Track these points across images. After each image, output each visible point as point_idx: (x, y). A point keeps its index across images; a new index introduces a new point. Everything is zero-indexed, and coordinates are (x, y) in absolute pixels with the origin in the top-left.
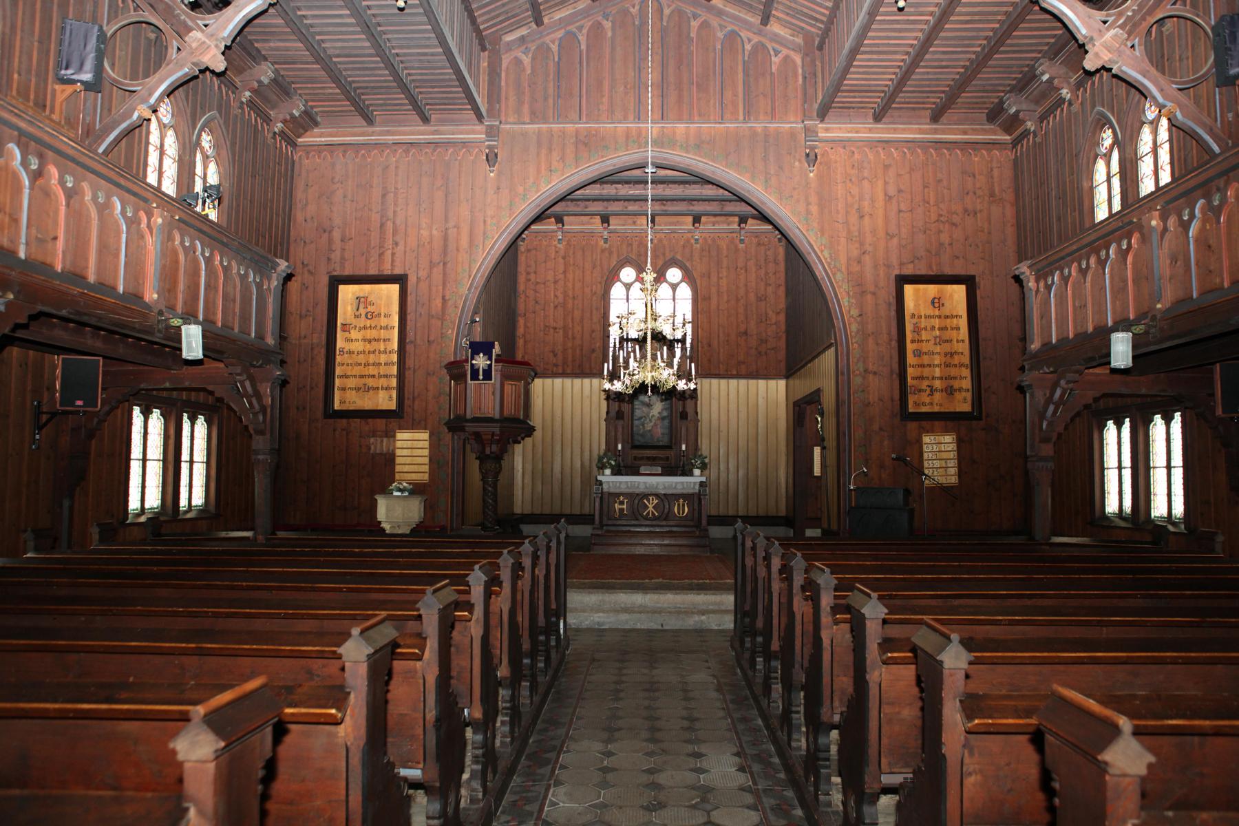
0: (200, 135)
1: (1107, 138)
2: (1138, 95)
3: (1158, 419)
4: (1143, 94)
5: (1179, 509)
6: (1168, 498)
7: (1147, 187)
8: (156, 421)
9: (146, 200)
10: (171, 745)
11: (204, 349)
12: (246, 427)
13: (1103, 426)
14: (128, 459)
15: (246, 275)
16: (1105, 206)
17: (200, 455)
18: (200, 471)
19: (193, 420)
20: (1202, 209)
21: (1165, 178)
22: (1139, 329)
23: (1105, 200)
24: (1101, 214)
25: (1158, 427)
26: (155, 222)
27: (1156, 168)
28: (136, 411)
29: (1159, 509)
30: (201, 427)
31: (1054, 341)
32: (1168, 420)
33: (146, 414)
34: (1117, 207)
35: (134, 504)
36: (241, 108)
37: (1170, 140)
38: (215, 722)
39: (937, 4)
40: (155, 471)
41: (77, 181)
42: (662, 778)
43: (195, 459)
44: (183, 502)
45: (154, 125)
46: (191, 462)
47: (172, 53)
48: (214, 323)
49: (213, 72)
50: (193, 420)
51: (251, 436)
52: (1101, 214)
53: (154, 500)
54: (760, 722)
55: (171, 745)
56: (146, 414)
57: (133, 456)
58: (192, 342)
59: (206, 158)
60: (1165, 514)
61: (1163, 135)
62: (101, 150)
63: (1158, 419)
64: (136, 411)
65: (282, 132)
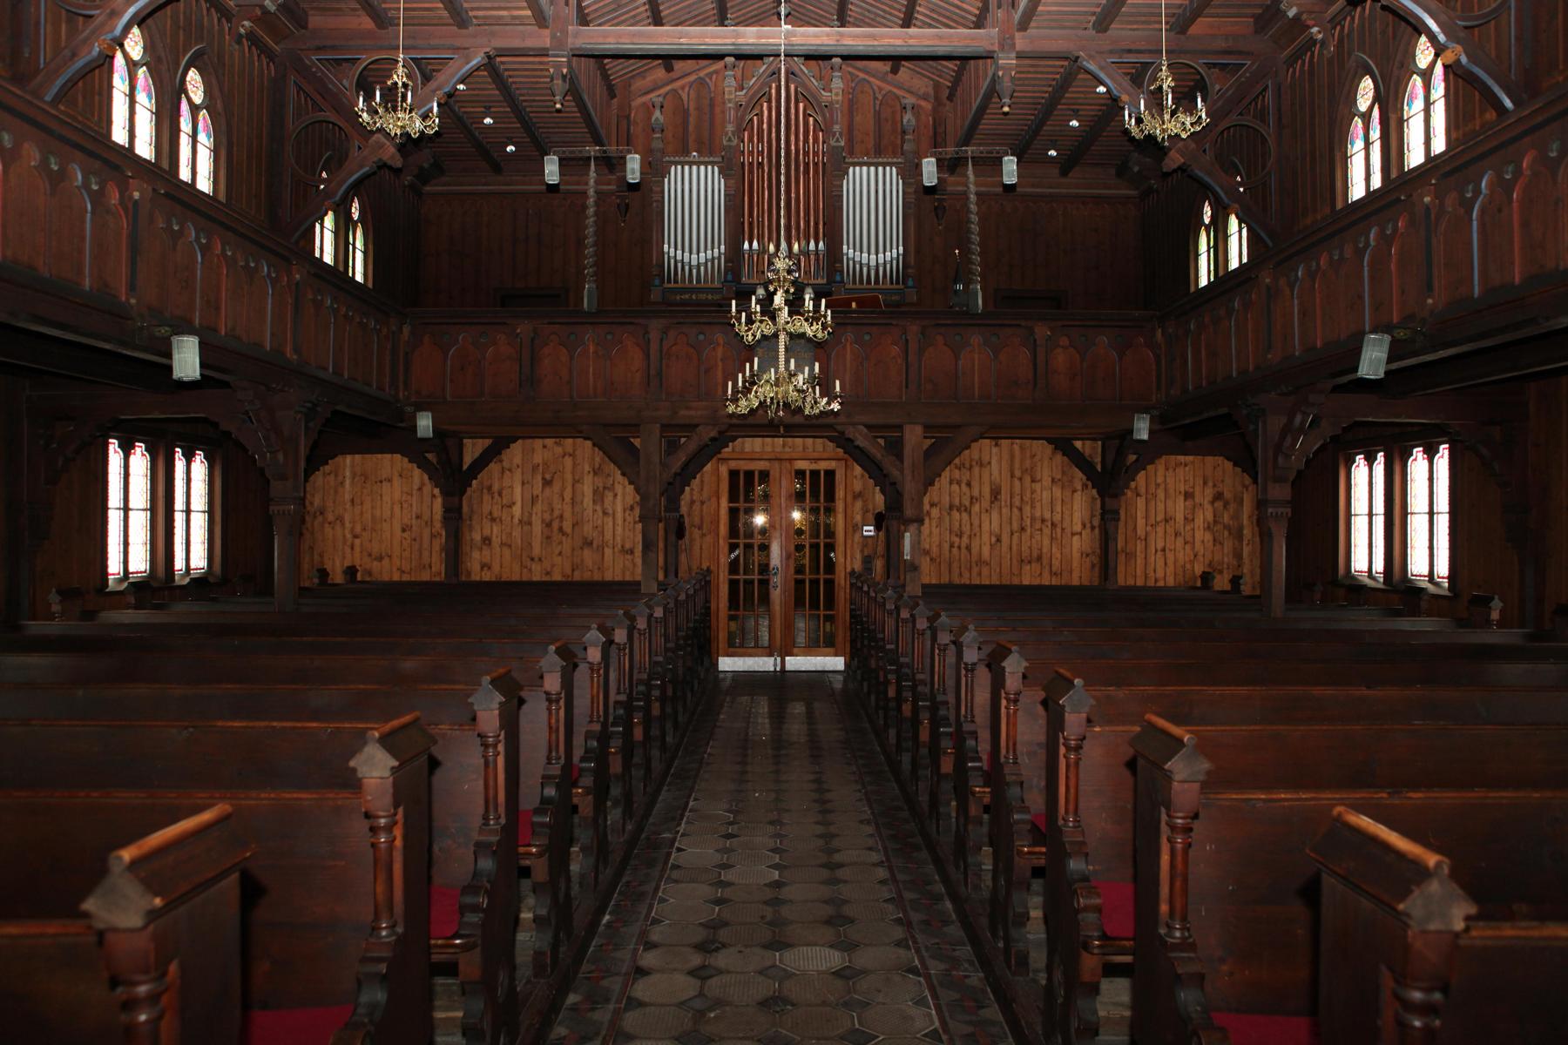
0: (127, 30)
1: (1366, 87)
2: (1410, 29)
3: (1418, 453)
4: (1419, 29)
5: (1442, 568)
6: (1429, 555)
7: (1415, 157)
8: (140, 461)
9: (116, 168)
10: (352, 764)
11: (202, 365)
12: (262, 470)
13: (1350, 462)
14: (105, 509)
15: (102, 192)
16: (1363, 184)
17: (199, 501)
18: (199, 522)
19: (189, 458)
20: (1490, 185)
21: (1439, 146)
22: (1155, 413)
23: (1362, 175)
24: (1357, 192)
25: (1418, 465)
26: (131, 197)
27: (1426, 131)
28: (114, 448)
29: (1418, 565)
30: (199, 468)
31: (1517, 280)
32: (1431, 453)
33: (127, 450)
34: (1376, 182)
35: (114, 566)
36: (239, 42)
37: (1446, 96)
38: (386, 741)
39: (1098, 5)
40: (140, 523)
41: (209, 238)
42: (786, 893)
43: (193, 507)
44: (179, 564)
45: (119, 60)
46: (188, 511)
47: (354, 153)
48: (215, 330)
49: (390, 168)
50: (189, 458)
51: (268, 482)
52: (1357, 192)
53: (139, 562)
54: (949, 905)
55: (352, 764)
56: (127, 450)
57: (110, 504)
58: (187, 360)
59: (195, 109)
60: (1426, 571)
61: (1439, 90)
62: (48, 98)
63: (1418, 453)
64: (114, 448)
65: (250, 35)
